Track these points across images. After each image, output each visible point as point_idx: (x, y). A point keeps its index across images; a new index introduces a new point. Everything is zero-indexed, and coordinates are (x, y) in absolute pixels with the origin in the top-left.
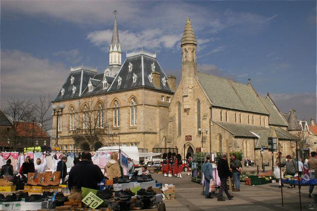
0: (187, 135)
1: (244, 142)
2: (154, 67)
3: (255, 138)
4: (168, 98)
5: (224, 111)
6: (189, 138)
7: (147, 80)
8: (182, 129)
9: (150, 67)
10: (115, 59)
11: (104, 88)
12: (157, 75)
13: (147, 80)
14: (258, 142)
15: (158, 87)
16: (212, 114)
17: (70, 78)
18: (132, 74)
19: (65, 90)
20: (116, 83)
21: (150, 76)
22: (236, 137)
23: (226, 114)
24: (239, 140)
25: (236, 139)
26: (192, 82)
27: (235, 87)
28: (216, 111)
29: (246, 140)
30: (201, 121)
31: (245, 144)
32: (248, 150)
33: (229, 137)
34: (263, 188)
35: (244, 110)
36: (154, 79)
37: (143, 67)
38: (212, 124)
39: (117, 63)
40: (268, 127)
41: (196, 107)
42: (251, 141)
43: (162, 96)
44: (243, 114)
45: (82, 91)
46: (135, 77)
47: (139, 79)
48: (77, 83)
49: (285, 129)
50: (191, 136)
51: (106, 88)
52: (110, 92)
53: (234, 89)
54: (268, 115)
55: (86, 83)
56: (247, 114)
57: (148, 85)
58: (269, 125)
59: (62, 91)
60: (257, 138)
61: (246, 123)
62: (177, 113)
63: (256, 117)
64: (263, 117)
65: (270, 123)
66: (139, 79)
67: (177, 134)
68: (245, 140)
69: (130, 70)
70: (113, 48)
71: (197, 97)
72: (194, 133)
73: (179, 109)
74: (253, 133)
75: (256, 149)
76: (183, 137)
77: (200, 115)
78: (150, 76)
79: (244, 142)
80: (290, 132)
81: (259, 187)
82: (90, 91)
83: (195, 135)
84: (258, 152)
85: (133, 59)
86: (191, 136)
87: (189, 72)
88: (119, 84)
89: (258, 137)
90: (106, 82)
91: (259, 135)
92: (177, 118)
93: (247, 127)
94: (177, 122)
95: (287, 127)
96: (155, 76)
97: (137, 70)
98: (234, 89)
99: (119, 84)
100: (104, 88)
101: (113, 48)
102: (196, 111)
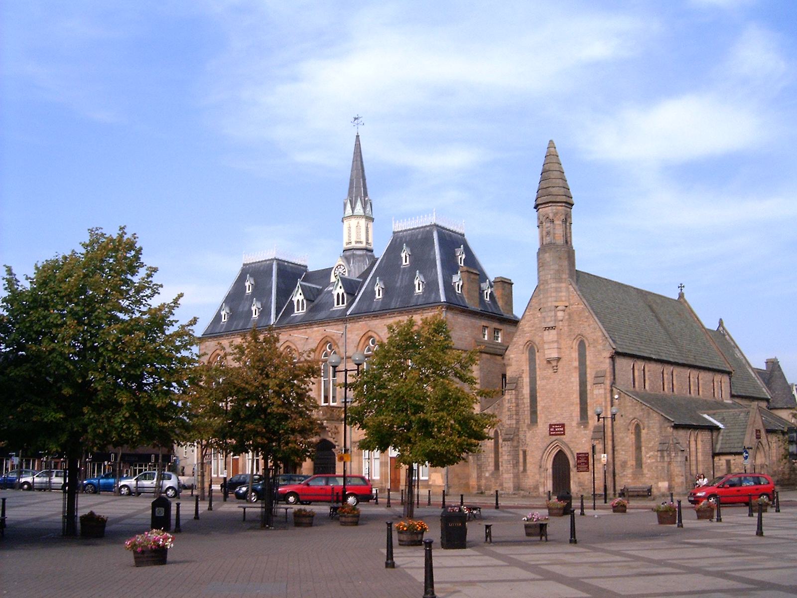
0: (554, 422)
1: (692, 439)
2: (464, 257)
3: (713, 429)
4: (496, 330)
5: (640, 364)
6: (557, 429)
7: (449, 287)
8: (539, 408)
9: (454, 257)
10: (349, 236)
11: (336, 307)
12: (473, 276)
13: (449, 287)
14: (720, 438)
15: (473, 305)
16: (616, 372)
17: (241, 279)
18: (410, 273)
19: (231, 310)
20: (370, 293)
21: (456, 279)
22: (676, 427)
23: (644, 370)
24: (682, 433)
25: (675, 432)
26: (564, 294)
27: (654, 306)
28: (624, 364)
29: (689, 432)
30: (589, 387)
31: (693, 443)
32: (700, 458)
33: (661, 427)
34: (525, 566)
35: (681, 362)
36: (465, 286)
37: (438, 257)
38: (616, 397)
39: (364, 245)
40: (728, 401)
41: (575, 355)
42: (704, 436)
43: (485, 327)
44: (677, 370)
45: (277, 315)
46: (418, 281)
47: (431, 286)
48: (261, 292)
49: (764, 405)
50: (563, 425)
51: (342, 306)
52: (357, 316)
53: (653, 311)
54: (729, 373)
55: (285, 293)
56: (688, 371)
57: (454, 300)
58: (732, 396)
59: (223, 313)
60: (717, 429)
61: (685, 392)
62: (526, 368)
63: (705, 376)
64: (718, 377)
65: (733, 393)
66: (431, 286)
67: (528, 421)
68: (694, 433)
69: (405, 263)
70: (353, 209)
71: (577, 332)
72: (570, 414)
73: (532, 361)
74: (706, 416)
75: (715, 455)
76: (542, 427)
77: (585, 374)
78: (456, 279)
79: (692, 439)
80: (772, 411)
81: (513, 562)
82: (299, 313)
83: (574, 424)
84: (722, 461)
85: (412, 235)
86: (563, 425)
87: (558, 271)
88: (379, 297)
89: (721, 426)
90: (341, 291)
91: (722, 421)
92: (526, 380)
93: (691, 401)
94: (526, 391)
95: (767, 400)
96: (469, 278)
97: (422, 262)
98: (653, 311)
99: (379, 297)
100: (336, 307)
101: (353, 209)
102: (576, 364)
